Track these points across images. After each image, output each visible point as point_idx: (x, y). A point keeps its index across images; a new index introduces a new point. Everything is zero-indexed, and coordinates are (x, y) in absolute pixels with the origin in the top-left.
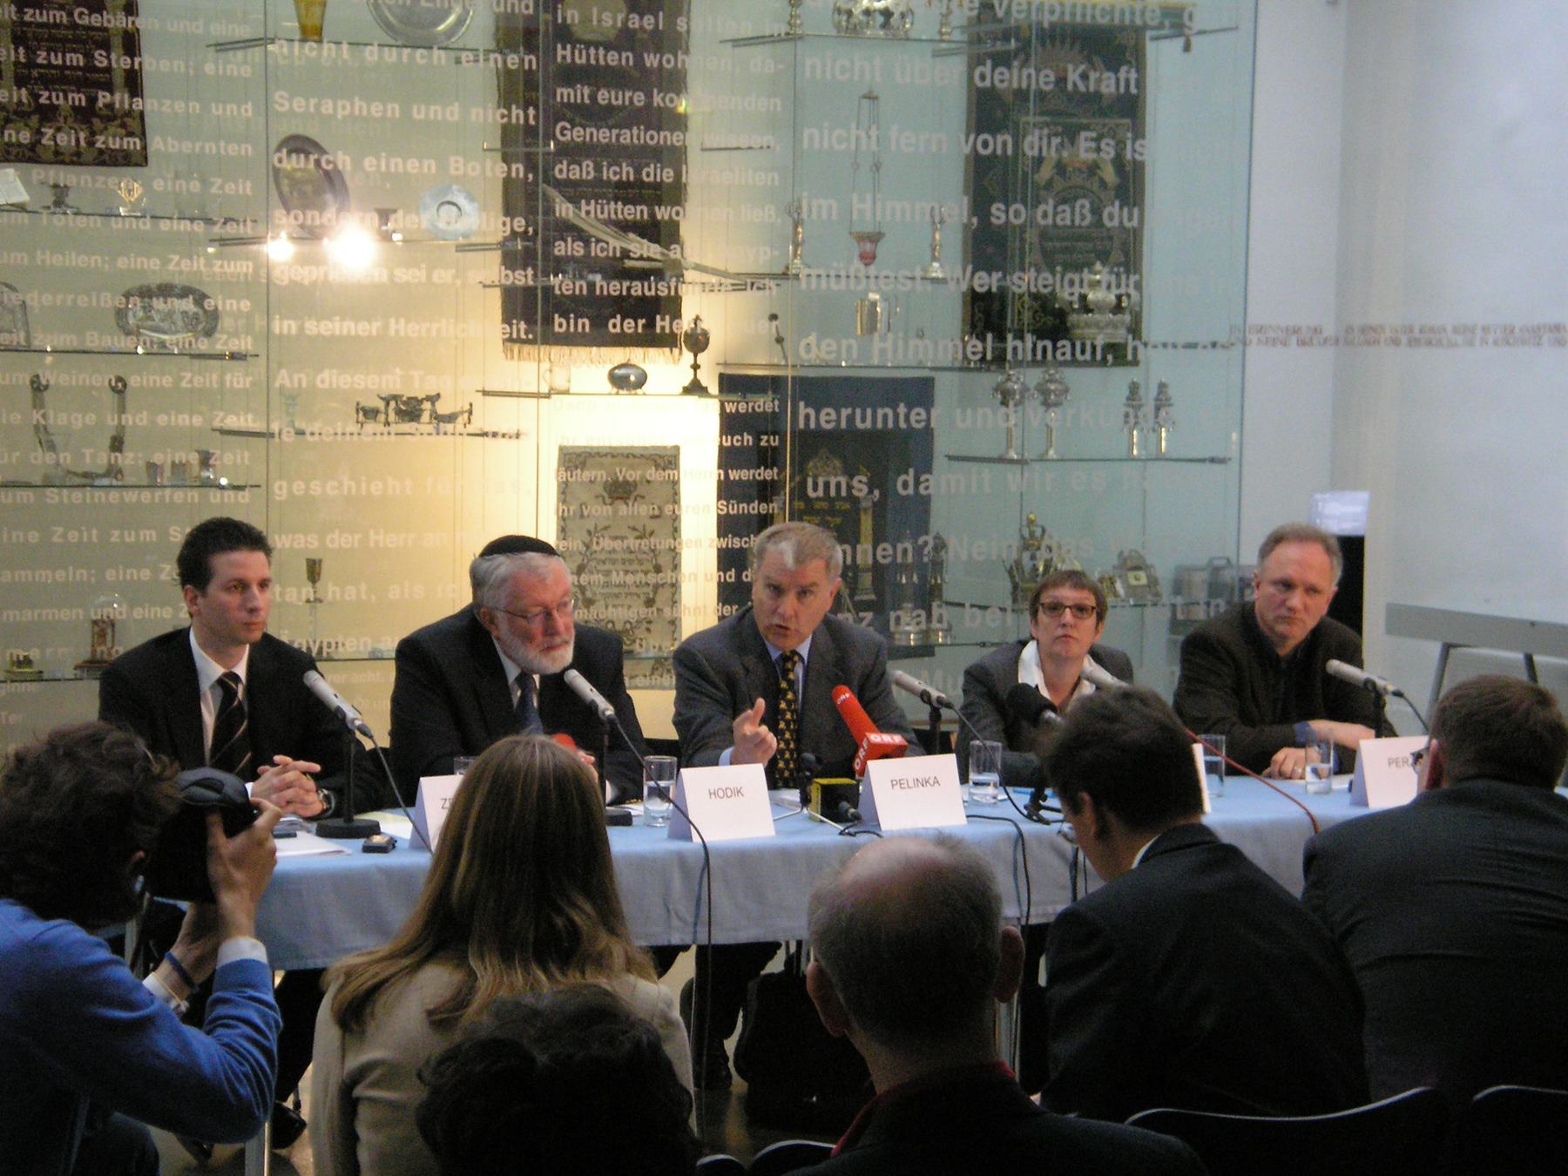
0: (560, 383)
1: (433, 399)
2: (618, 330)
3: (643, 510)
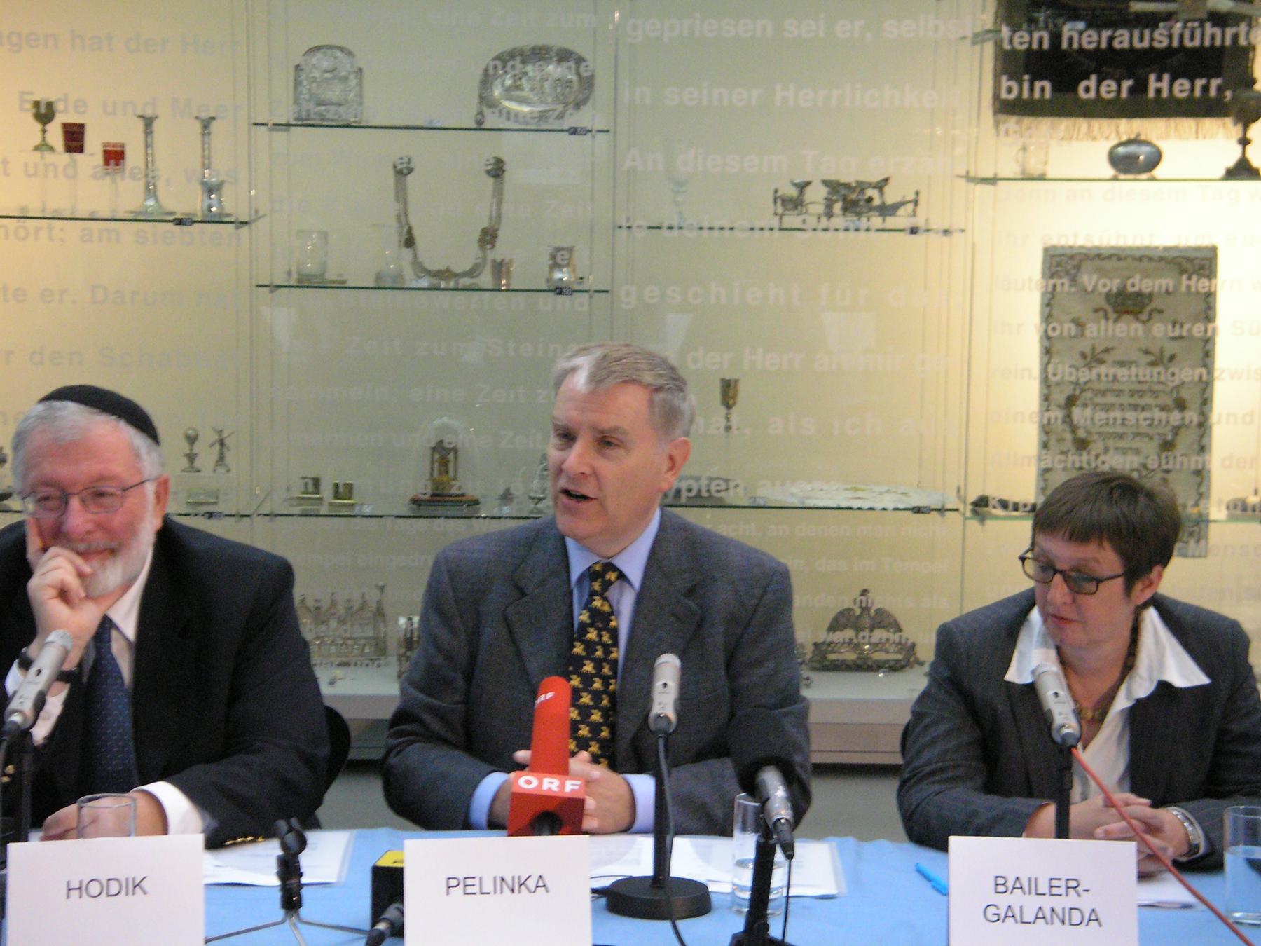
0: (1034, 167)
1: (881, 185)
2: (1092, 95)
3: (1159, 329)
